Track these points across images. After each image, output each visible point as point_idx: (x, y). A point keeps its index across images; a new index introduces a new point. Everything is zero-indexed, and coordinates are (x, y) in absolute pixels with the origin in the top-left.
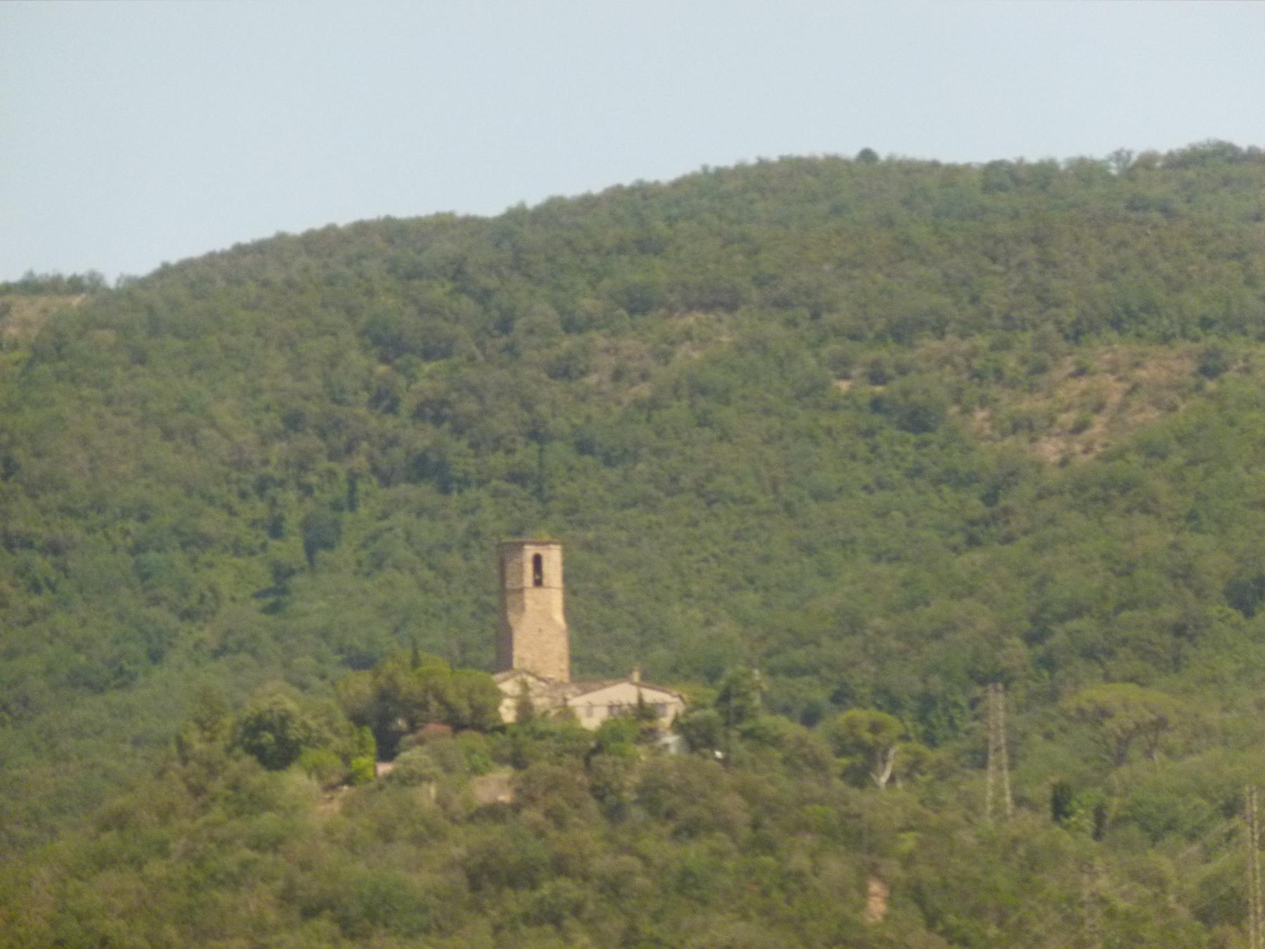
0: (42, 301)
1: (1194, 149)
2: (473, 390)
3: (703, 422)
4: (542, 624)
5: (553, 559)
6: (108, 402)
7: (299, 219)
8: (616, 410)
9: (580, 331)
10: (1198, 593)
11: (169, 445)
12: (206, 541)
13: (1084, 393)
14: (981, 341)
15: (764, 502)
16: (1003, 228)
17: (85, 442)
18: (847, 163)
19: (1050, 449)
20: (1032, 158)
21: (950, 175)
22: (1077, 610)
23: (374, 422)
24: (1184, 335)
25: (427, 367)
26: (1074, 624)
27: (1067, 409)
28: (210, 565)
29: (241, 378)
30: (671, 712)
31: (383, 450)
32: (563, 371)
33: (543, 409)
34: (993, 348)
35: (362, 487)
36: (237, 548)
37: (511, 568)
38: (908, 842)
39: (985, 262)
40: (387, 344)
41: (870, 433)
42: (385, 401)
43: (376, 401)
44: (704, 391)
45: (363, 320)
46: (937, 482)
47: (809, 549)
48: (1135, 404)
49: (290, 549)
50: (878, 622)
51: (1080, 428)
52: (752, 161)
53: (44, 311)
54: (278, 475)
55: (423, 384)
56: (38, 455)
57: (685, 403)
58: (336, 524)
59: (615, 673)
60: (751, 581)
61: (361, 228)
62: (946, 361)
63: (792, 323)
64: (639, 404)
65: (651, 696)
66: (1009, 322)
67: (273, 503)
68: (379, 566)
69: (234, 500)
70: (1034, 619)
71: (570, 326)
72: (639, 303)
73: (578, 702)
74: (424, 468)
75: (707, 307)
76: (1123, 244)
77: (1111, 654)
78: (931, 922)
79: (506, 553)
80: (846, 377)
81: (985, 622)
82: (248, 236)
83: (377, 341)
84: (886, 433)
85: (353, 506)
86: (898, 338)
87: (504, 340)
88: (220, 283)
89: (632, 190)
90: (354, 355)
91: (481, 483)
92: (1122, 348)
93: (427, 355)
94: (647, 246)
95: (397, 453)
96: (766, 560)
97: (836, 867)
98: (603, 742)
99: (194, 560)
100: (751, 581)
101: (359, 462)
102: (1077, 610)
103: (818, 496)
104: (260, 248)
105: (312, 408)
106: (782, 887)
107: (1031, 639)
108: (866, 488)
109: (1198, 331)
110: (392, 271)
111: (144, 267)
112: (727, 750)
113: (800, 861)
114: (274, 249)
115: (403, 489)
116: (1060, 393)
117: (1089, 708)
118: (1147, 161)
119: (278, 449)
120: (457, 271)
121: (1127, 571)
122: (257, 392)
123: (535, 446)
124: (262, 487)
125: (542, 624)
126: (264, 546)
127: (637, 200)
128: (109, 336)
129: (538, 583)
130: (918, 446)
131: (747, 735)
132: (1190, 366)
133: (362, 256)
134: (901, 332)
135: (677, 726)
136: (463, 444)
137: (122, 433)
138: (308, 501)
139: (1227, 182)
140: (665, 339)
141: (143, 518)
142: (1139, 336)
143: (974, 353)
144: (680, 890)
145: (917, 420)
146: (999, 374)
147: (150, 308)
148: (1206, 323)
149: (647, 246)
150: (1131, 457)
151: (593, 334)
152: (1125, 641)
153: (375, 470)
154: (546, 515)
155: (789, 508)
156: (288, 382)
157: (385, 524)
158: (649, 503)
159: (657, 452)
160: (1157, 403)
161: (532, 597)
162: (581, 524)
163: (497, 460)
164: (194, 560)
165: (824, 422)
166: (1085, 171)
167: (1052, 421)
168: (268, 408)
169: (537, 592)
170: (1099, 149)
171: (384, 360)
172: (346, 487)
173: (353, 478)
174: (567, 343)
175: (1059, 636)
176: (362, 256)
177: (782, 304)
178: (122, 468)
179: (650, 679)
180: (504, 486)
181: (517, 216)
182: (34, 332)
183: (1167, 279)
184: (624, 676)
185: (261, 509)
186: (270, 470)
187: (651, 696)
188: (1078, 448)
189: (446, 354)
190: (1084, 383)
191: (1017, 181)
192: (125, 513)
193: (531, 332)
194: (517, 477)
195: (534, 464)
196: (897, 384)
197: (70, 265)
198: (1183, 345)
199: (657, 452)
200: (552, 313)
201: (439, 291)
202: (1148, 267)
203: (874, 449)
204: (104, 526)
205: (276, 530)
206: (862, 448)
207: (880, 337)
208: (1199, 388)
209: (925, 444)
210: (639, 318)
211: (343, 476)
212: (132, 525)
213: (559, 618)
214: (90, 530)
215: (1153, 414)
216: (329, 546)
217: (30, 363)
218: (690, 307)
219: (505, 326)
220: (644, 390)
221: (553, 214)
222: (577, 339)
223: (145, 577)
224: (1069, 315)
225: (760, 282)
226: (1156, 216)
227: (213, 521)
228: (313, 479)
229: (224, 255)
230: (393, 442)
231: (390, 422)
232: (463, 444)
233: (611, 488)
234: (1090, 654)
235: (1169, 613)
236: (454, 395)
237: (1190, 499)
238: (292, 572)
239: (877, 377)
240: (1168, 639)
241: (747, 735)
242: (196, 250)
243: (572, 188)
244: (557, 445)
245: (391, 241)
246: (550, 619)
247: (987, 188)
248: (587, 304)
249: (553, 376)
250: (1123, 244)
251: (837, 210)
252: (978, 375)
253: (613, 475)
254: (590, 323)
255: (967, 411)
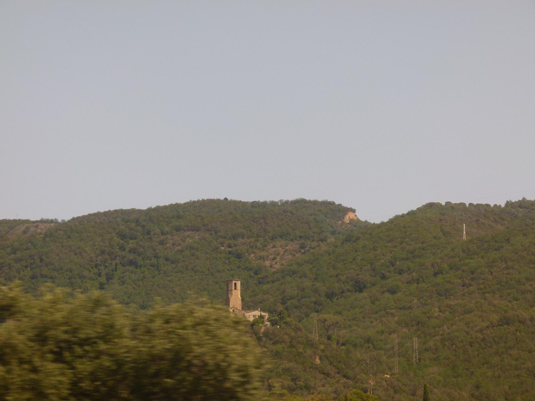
0: (45, 225)
1: (297, 200)
2: (142, 247)
3: (193, 255)
4: (236, 298)
5: (239, 284)
6: (62, 247)
7: (102, 209)
8: (174, 252)
9: (165, 235)
10: (319, 295)
11: (76, 256)
12: (85, 277)
13: (275, 251)
14: (253, 240)
15: (207, 272)
16: (256, 216)
17: (58, 255)
18: (221, 200)
19: (268, 263)
20: (262, 200)
21: (244, 204)
22: (292, 298)
23: (120, 253)
24: (296, 239)
25: (131, 241)
26: (292, 301)
27: (271, 255)
28: (85, 282)
29: (91, 242)
30: (267, 317)
31: (123, 259)
32: (161, 243)
33: (158, 251)
34: (255, 241)
35: (118, 267)
36: (91, 279)
37: (230, 285)
38: (322, 347)
39: (252, 223)
40: (123, 236)
41: (229, 259)
42: (122, 248)
43: (120, 248)
44: (193, 249)
45: (117, 231)
46: (243, 270)
47: (217, 283)
48: (286, 254)
49: (103, 279)
50: (247, 299)
51: (274, 259)
52: (201, 199)
53: (46, 227)
54: (100, 264)
55: (131, 245)
56: (48, 258)
57: (189, 251)
58: (113, 274)
59: (254, 309)
60: (205, 289)
61: (116, 211)
62: (244, 244)
63: (211, 234)
64: (179, 251)
65: (263, 314)
66: (258, 236)
67: (99, 269)
68: (123, 284)
69: (90, 268)
70: (282, 300)
71: (163, 233)
72: (178, 229)
73: (247, 315)
74: (132, 263)
75: (193, 231)
76: (282, 220)
77: (301, 307)
78: (331, 364)
79: (228, 283)
80: (223, 246)
81: (272, 300)
82: (91, 212)
83: (120, 235)
84: (232, 259)
85: (116, 271)
86: (234, 239)
87: (148, 236)
88: (86, 222)
89: (175, 205)
90: (115, 238)
91: (145, 267)
92: (283, 242)
93: (131, 239)
94: (179, 217)
95: (126, 259)
96: (207, 285)
97: (309, 352)
98: (253, 325)
99: (82, 281)
100: (205, 289)
101: (117, 261)
102: (292, 298)
103: (218, 271)
104: (94, 215)
105: (107, 249)
106: (298, 355)
107: (283, 304)
108: (228, 270)
109: (298, 238)
110: (123, 220)
111: (67, 218)
112: (280, 326)
113: (301, 350)
114: (97, 215)
115: (128, 267)
116: (270, 251)
117: (322, 319)
118: (287, 202)
119: (100, 258)
120: (137, 221)
121: (303, 290)
122: (94, 246)
123: (156, 259)
124: (96, 266)
125: (236, 298)
126: (97, 279)
127: (175, 207)
128: (62, 232)
129: (235, 289)
130: (239, 262)
131: (284, 323)
132: (298, 246)
133: (116, 217)
134: (235, 237)
135: (269, 320)
136: (140, 258)
137: (66, 253)
138: (106, 270)
139: (304, 207)
140: (184, 237)
141: (71, 272)
142: (286, 239)
143: (251, 242)
144: (276, 355)
145: (239, 256)
146: (256, 247)
147: (71, 227)
148: (301, 237)
149: (179, 217)
150: (294, 265)
151: (168, 236)
152: (304, 305)
153: (121, 263)
154: (159, 274)
155: (212, 274)
156: (101, 244)
157: (124, 275)
158: (182, 272)
159: (183, 261)
160: (291, 254)
161: (234, 292)
162: (167, 276)
163: (148, 262)
164: (82, 281)
165: (219, 256)
166: (273, 204)
167: (268, 257)
168: (97, 249)
169: (235, 291)
170: (276, 199)
171: (122, 239)
172: (115, 267)
173: (116, 265)
174: (162, 237)
175: (289, 303)
176: (116, 217)
177: (209, 230)
178: (66, 261)
179: (263, 310)
180: (150, 267)
181: (150, 209)
182: (44, 231)
183: (292, 227)
184: (257, 309)
185: (96, 271)
186: (98, 262)
187: (263, 314)
188: (274, 263)
189: (135, 239)
190: (275, 249)
191: (259, 206)
192: (67, 271)
193: (155, 235)
194: (152, 266)
195: (156, 263)
196: (234, 248)
197: (51, 217)
198: (296, 242)
199: (183, 261)
200: (159, 231)
201: (133, 225)
202: (288, 225)
203: (230, 262)
204: (62, 273)
205: (100, 275)
206: (227, 261)
207: (230, 239)
208: (300, 251)
209: (241, 261)
210: (178, 232)
211: (114, 264)
212: (69, 273)
213: (240, 296)
214: (59, 274)
215: (290, 256)
216: (111, 279)
217: (45, 238)
218: (189, 230)
219: (148, 233)
220: (179, 248)
221: (158, 209)
222: (165, 236)
223: (72, 285)
224: (271, 235)
225: (204, 225)
226: (289, 214)
227: (86, 273)
228: (107, 265)
229: (86, 216)
230: (125, 257)
231: (124, 253)
232: (140, 258)
233: (174, 269)
234: (296, 307)
235: (313, 299)
236: (138, 248)
237: (314, 275)
238: (104, 284)
239: (230, 246)
240: (313, 305)
241: (284, 323)
242: (81, 215)
243: (162, 204)
244: (161, 259)
245: (122, 214)
246: (238, 297)
247: (252, 207)
248: (167, 229)
249: (160, 244)
250: (282, 220)
251: (220, 211)
252: (252, 247)
253: (174, 266)
254: (167, 233)
255: (249, 254)
